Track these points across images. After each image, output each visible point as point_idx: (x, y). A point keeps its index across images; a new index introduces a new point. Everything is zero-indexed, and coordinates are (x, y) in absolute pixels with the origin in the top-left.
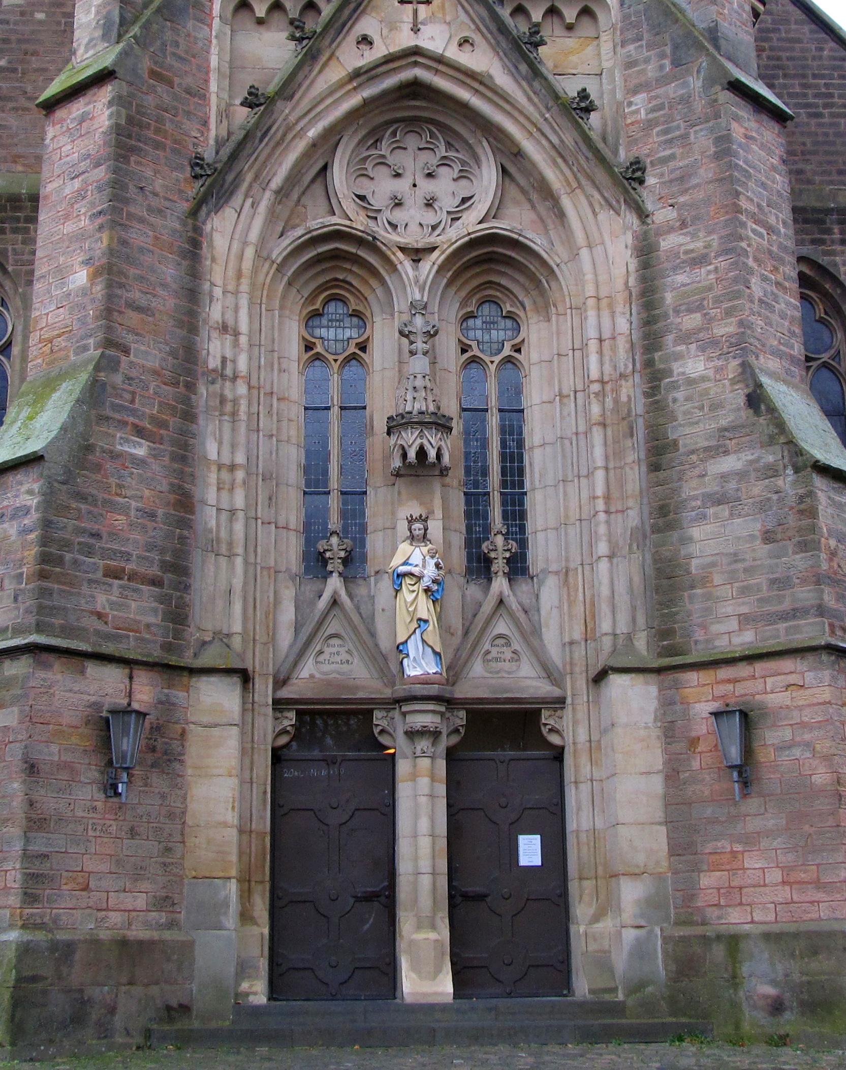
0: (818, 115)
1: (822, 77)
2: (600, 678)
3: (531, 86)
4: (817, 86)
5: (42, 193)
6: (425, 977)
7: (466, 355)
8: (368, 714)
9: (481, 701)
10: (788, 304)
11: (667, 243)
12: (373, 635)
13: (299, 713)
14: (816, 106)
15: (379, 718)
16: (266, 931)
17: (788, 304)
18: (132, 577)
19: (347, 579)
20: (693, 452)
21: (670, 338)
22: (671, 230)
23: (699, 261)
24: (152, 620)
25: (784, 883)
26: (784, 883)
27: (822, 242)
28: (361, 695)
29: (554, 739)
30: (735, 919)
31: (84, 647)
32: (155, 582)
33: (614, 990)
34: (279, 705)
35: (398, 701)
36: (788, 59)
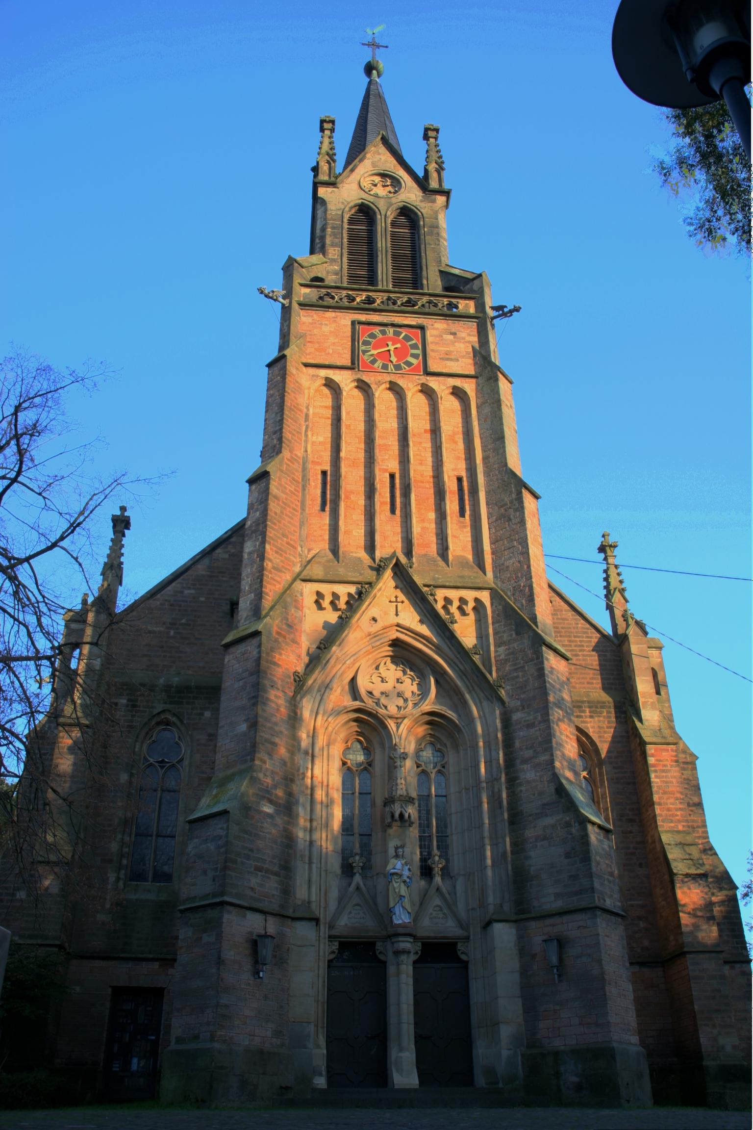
0: (577, 655)
1: (579, 637)
2: (488, 925)
3: (451, 642)
4: (576, 641)
5: (223, 686)
6: (405, 1074)
7: (420, 769)
8: (373, 944)
9: (429, 938)
10: (572, 746)
11: (516, 716)
12: (375, 904)
13: (340, 943)
14: (575, 650)
15: (379, 946)
16: (325, 1051)
17: (572, 746)
18: (267, 871)
19: (364, 877)
20: (530, 815)
21: (518, 761)
22: (517, 710)
23: (530, 726)
24: (275, 893)
25: (580, 1024)
26: (580, 1024)
27: (581, 717)
28: (370, 934)
29: (464, 957)
30: (557, 1043)
31: (245, 904)
32: (276, 874)
33: (498, 1083)
34: (331, 938)
35: (390, 937)
36: (563, 628)
